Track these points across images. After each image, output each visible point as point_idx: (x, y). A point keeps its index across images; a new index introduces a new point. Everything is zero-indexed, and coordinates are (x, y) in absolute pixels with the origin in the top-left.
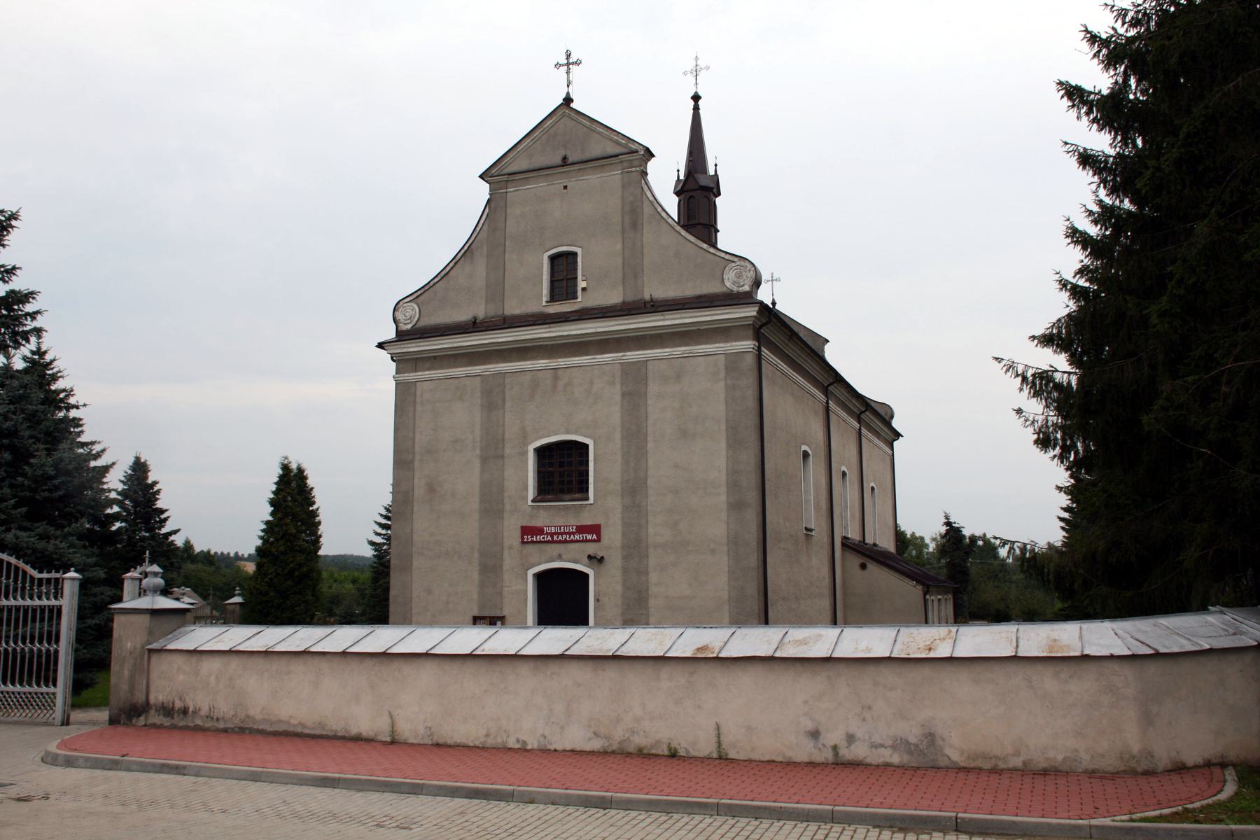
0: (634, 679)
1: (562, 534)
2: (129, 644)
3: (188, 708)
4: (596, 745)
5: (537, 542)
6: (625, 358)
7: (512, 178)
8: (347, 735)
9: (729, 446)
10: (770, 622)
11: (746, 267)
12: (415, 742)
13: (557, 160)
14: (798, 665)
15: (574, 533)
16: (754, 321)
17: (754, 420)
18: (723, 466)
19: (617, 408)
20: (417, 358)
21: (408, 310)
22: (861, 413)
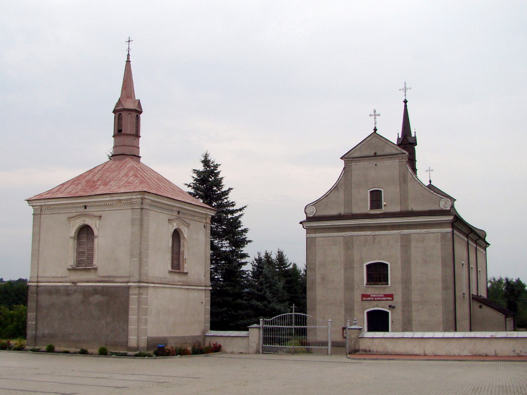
0: (478, 342)
1: (378, 297)
4: (470, 354)
5: (368, 300)
7: (353, 159)
9: (442, 266)
10: (457, 330)
13: (373, 154)
15: (383, 297)
17: (451, 258)
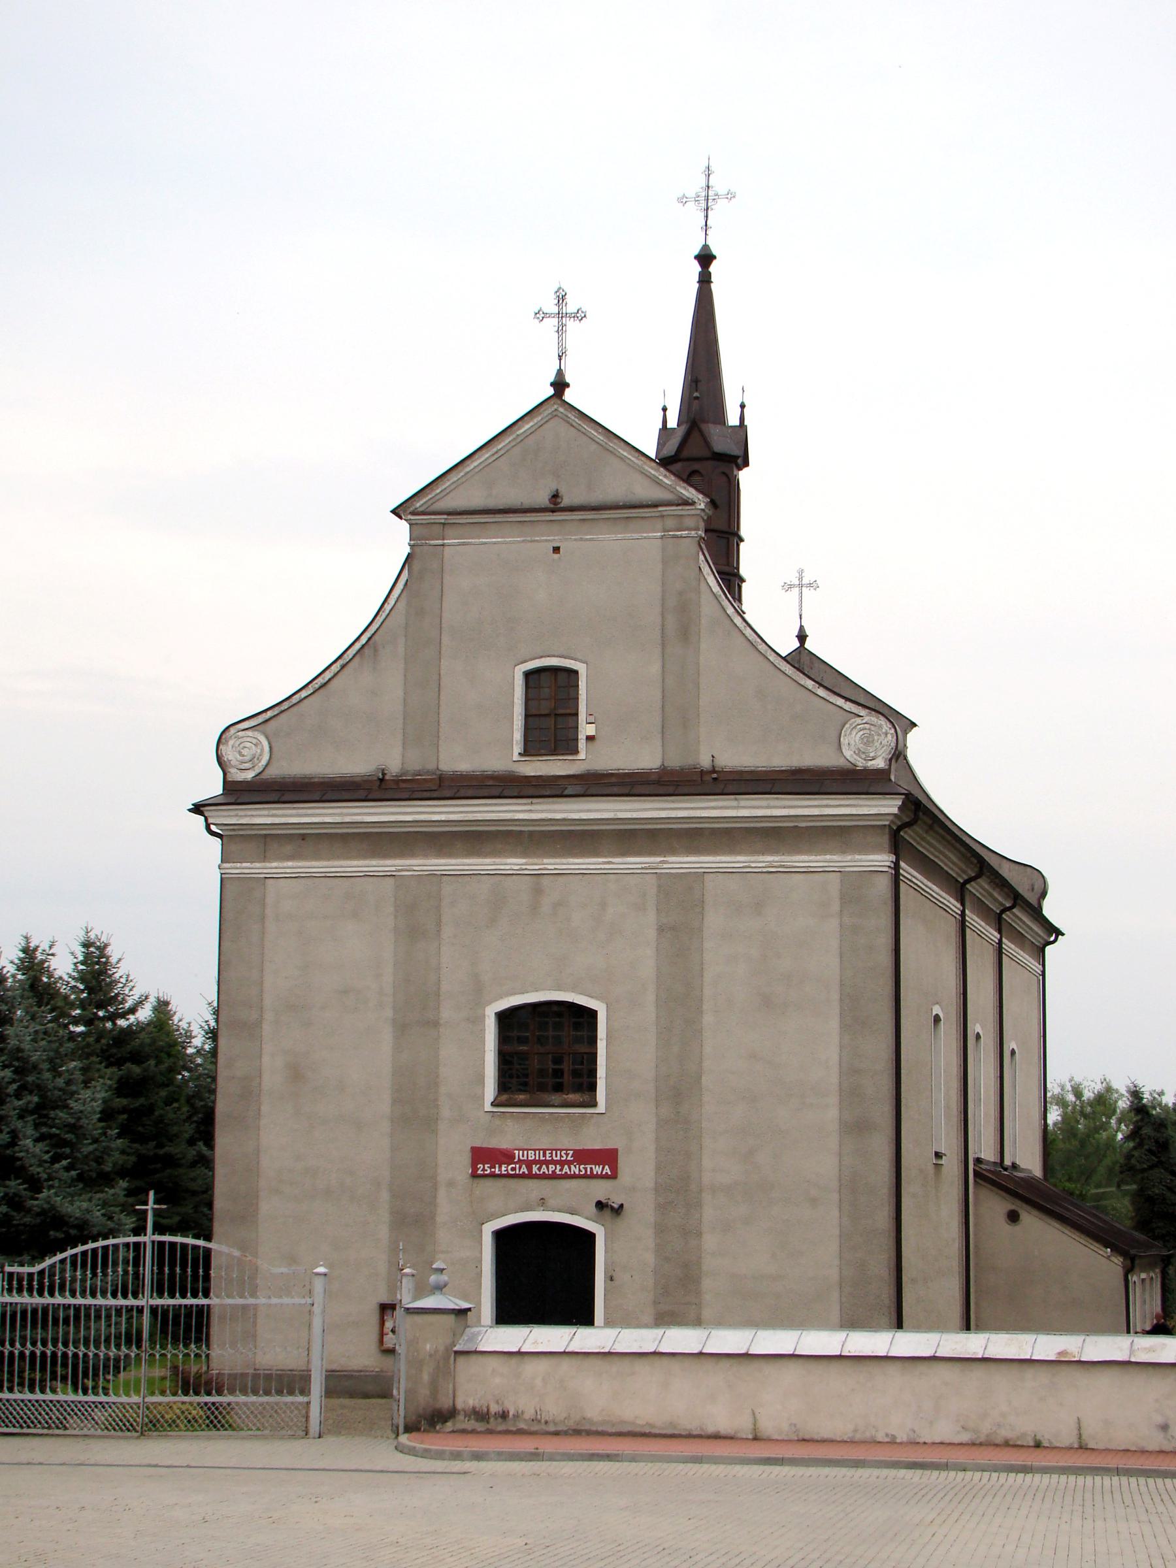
0: (1001, 1380)
1: (547, 1163)
2: (428, 1347)
3: (508, 1412)
4: (965, 1437)
5: (501, 1176)
6: (665, 866)
8: (703, 1434)
9: (844, 1027)
11: (881, 726)
12: (779, 1438)
14: (1150, 1368)
15: (569, 1163)
16: (892, 822)
18: (835, 1058)
19: (650, 952)
20: (266, 836)
21: (248, 745)
22: (1003, 911)
